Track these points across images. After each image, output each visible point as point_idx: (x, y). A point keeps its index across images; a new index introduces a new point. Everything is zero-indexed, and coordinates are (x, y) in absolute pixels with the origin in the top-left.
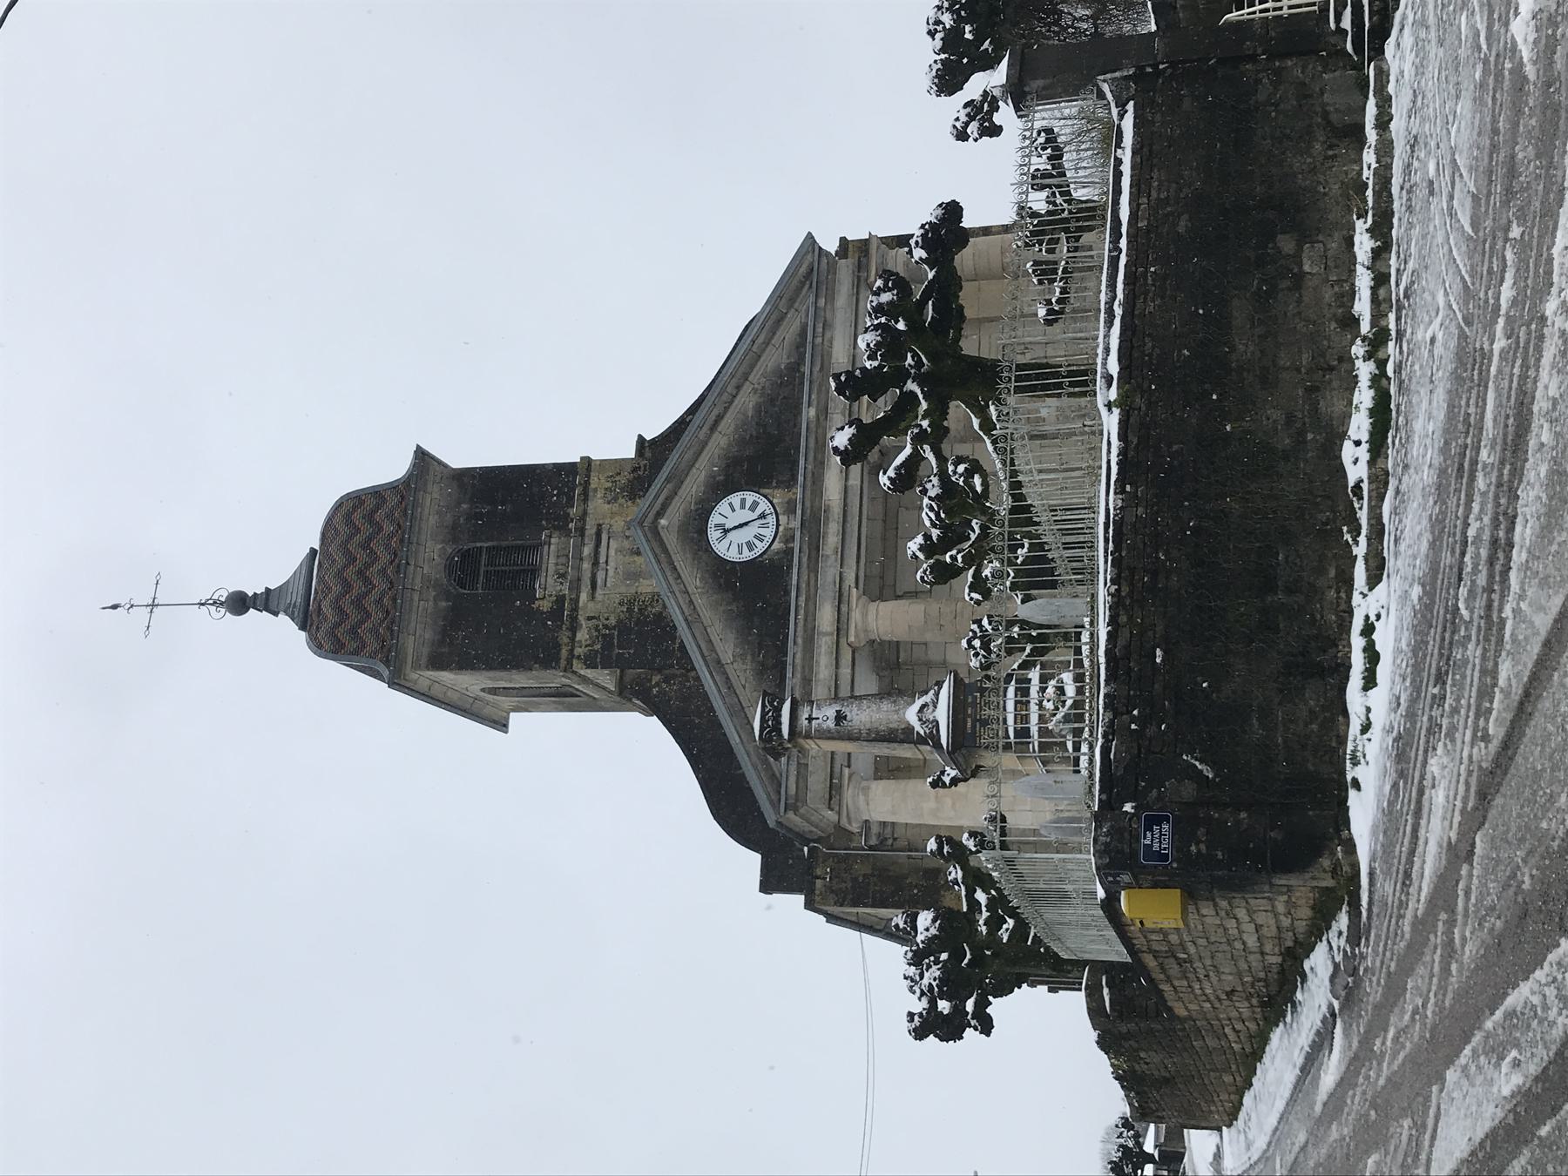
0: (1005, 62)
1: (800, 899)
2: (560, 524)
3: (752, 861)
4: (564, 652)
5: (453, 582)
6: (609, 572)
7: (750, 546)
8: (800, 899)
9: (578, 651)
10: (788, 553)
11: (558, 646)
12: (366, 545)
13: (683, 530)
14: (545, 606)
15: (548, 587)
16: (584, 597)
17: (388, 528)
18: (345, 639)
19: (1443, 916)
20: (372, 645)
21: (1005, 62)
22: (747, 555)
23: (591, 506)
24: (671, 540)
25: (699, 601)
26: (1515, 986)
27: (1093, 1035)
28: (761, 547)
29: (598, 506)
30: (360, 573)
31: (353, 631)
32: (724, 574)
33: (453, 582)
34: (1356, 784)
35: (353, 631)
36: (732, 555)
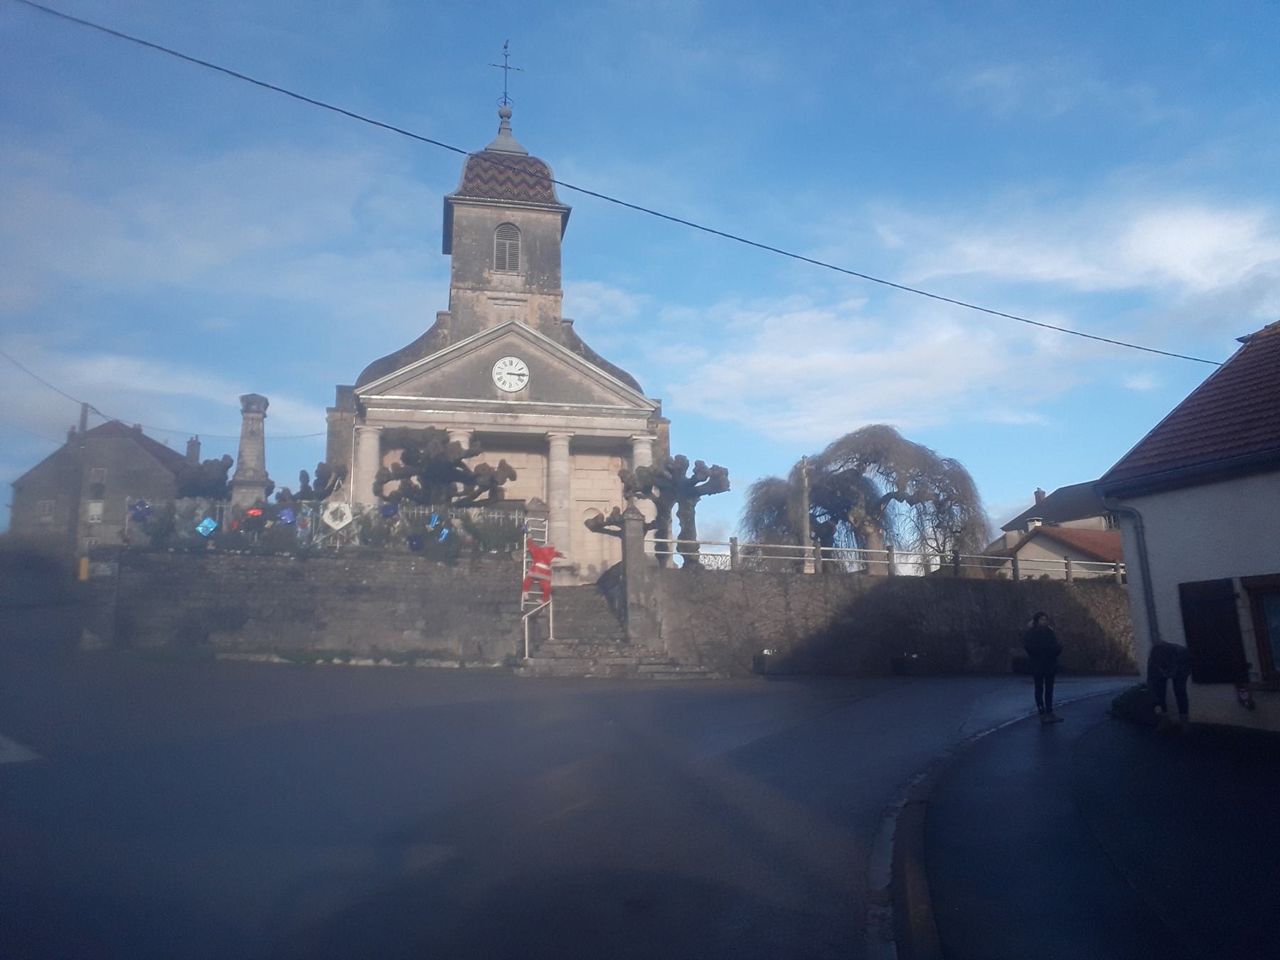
1: (334, 406)
4: (461, 285)
5: (1062, 720)
7: (500, 379)
8: (334, 406)
10: (496, 398)
11: (464, 281)
12: (523, 181)
13: (511, 345)
14: (486, 275)
15: (497, 277)
19: (420, 663)
22: (495, 377)
27: (782, 472)
28: (499, 384)
29: (538, 299)
30: (508, 179)
31: (478, 176)
32: (486, 366)
33: (1062, 720)
35: (478, 176)
36: (496, 369)
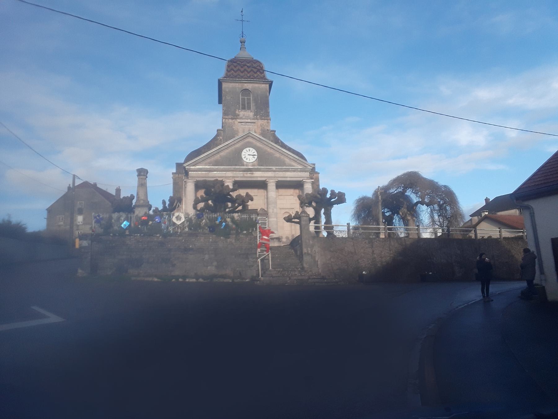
0: (159, 280)
2: (256, 114)
3: (98, 186)
4: (227, 117)
6: (246, 123)
9: (227, 120)
10: (243, 165)
11: (228, 115)
13: (249, 142)
15: (242, 113)
16: (239, 120)
17: (255, 75)
18: (231, 68)
20: (229, 74)
21: (159, 280)
22: (243, 157)
23: (260, 121)
24: (247, 140)
25: (233, 148)
26: (342, 237)
28: (245, 160)
29: (260, 122)
31: (232, 69)
34: (393, 202)
35: (232, 69)
36: (243, 153)
